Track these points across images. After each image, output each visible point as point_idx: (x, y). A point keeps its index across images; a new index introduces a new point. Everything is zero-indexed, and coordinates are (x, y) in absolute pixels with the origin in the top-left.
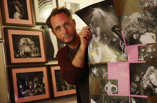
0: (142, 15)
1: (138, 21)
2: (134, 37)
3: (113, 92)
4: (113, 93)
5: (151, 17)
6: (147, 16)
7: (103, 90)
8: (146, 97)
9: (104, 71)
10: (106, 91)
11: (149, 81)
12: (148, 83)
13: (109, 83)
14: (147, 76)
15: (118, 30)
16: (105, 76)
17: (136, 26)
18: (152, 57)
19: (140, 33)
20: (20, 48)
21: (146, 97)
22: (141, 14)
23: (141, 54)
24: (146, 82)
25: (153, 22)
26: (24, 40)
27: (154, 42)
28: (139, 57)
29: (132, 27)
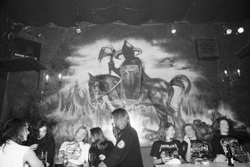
1: (87, 87)
20: (58, 113)
26: (102, 54)
29: (62, 110)
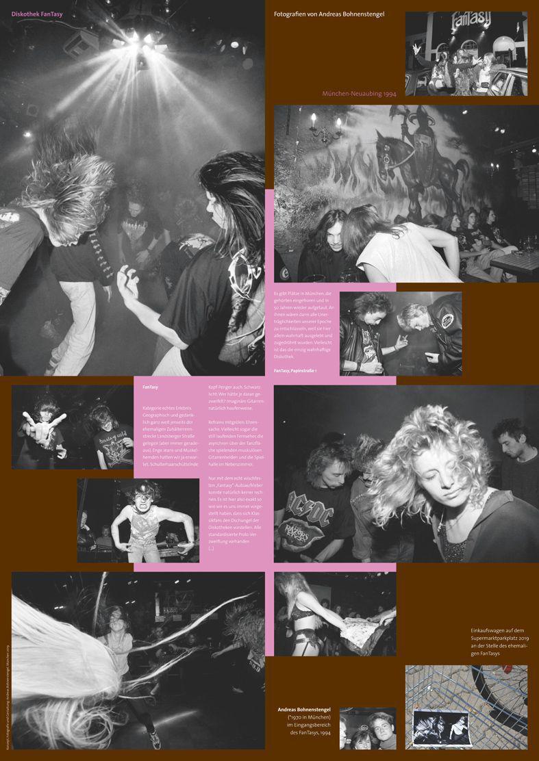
0: (405, 128)
1: (375, 152)
2: (330, 240)
3: (165, 553)
4: (168, 560)
5: (450, 142)
6: (432, 134)
7: (99, 541)
8: (389, 568)
9: (108, 426)
10: (119, 545)
11: (410, 485)
12: (402, 493)
13: (139, 499)
14: (396, 459)
15: (247, 186)
16: (117, 457)
17: (362, 178)
18: (435, 358)
19: (370, 221)
21: (389, 568)
22: (399, 119)
23: (360, 335)
24: (391, 490)
25: (456, 175)
27: (450, 276)
28: (349, 350)
29: (336, 180)
